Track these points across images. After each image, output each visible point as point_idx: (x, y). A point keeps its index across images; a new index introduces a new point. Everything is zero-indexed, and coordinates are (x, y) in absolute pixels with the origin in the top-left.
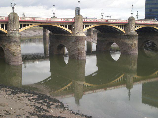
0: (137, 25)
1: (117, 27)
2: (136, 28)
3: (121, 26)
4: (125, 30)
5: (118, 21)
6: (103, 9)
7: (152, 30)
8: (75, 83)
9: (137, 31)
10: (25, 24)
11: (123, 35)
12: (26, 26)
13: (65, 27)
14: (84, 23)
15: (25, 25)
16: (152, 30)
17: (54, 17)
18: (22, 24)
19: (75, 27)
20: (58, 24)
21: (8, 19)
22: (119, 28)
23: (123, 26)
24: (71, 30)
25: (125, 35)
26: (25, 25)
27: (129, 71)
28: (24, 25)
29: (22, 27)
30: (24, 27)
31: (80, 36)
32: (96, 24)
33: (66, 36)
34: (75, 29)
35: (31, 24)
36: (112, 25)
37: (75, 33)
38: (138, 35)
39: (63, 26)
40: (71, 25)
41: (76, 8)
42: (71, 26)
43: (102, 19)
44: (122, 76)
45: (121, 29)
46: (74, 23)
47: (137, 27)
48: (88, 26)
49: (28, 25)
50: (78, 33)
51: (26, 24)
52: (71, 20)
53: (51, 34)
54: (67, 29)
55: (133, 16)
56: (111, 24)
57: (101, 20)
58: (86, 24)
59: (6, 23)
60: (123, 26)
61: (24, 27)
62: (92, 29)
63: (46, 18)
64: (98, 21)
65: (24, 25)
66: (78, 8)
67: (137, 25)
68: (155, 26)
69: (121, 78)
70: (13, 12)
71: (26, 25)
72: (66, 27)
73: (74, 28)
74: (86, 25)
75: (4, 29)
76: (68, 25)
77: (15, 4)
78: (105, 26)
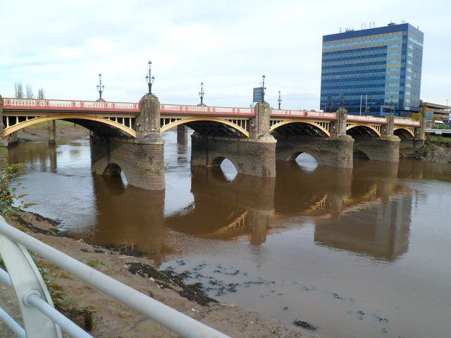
0: (273, 120)
1: (231, 124)
2: (271, 125)
3: (239, 121)
4: (381, 132)
5: (236, 111)
6: (102, 77)
7: (308, 131)
8: (255, 214)
9: (348, 132)
10: (167, 117)
11: (327, 139)
12: (170, 123)
13: (123, 124)
14: (272, 117)
15: (15, 118)
16: (308, 131)
17: (100, 100)
19: (257, 125)
21: (140, 108)
22: (236, 126)
23: (243, 121)
24: (248, 130)
25: (329, 141)
27: (335, 190)
28: (166, 119)
30: (10, 125)
31: (267, 142)
33: (218, 140)
34: (257, 128)
36: (94, 117)
37: (257, 135)
38: (276, 141)
39: (235, 122)
40: (248, 121)
41: (254, 89)
42: (133, 120)
43: (201, 104)
44: (243, 216)
45: (240, 129)
46: (255, 117)
47: (275, 123)
48: (279, 121)
49: (173, 120)
50: (262, 136)
51: (170, 117)
52: (130, 107)
53: (197, 137)
54: (240, 129)
55: (152, 92)
57: (98, 104)
58: (274, 119)
60: (243, 121)
61: (10, 125)
63: (72, 101)
64: (191, 110)
65: (166, 119)
66: (261, 88)
67: (273, 120)
69: (242, 221)
70: (150, 93)
72: (321, 125)
73: (255, 127)
74: (169, 119)
75: (130, 128)
77: (153, 78)
78: (301, 123)
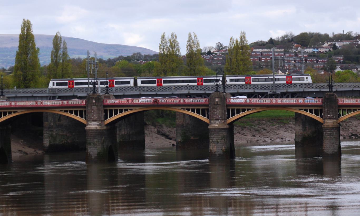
10: (239, 108)
15: (240, 109)
18: (235, 109)
20: (183, 108)
26: (240, 109)
28: (120, 110)
29: (240, 113)
30: (4, 116)
32: (137, 108)
35: (126, 108)
39: (193, 111)
51: (124, 108)
56: (175, 108)
59: (321, 108)
61: (109, 118)
62: (211, 95)
68: (180, 108)
71: (124, 111)
72: (76, 114)
74: (117, 110)
75: (206, 118)
76: (202, 109)
